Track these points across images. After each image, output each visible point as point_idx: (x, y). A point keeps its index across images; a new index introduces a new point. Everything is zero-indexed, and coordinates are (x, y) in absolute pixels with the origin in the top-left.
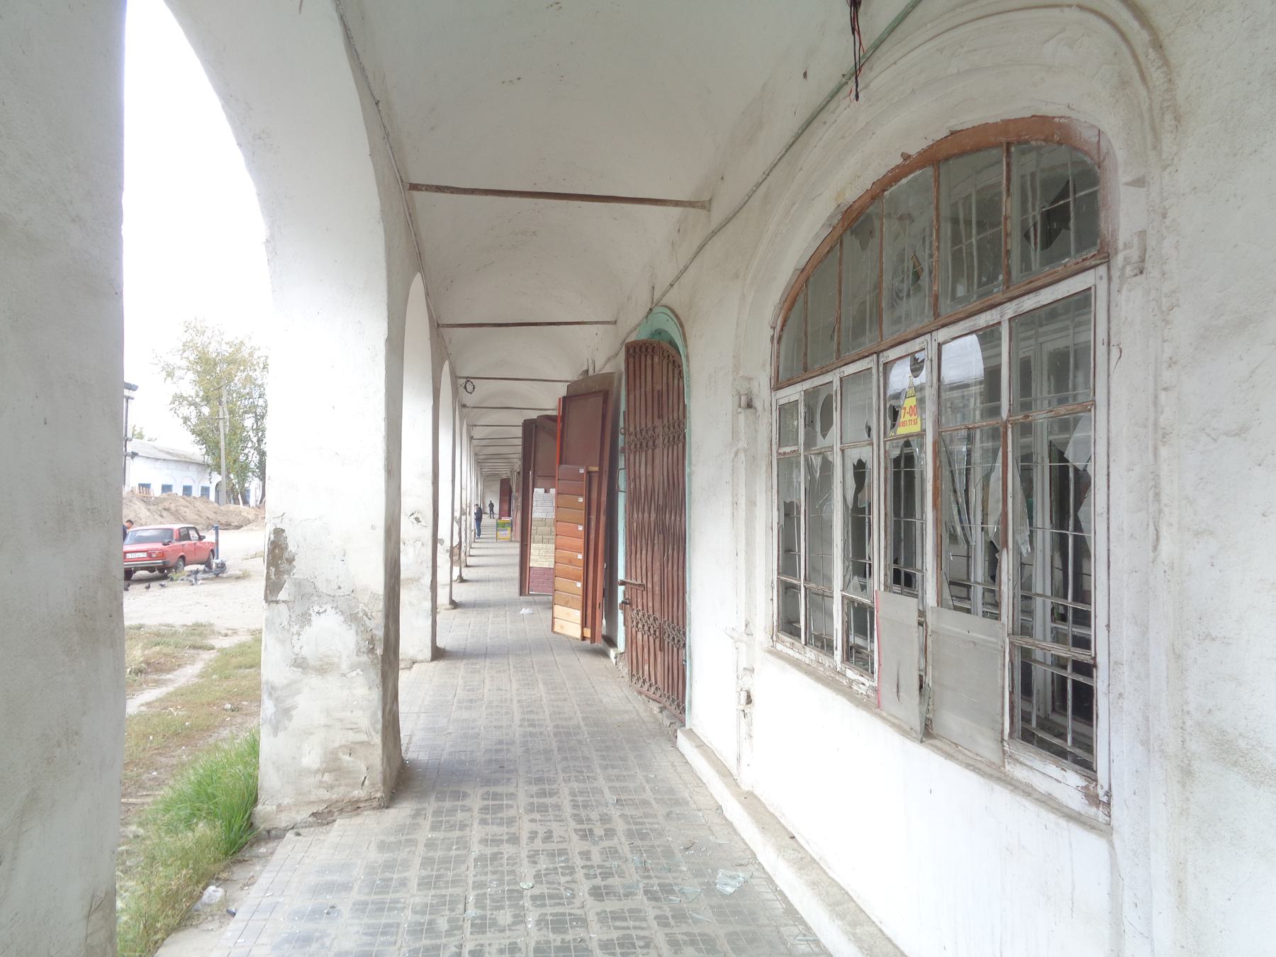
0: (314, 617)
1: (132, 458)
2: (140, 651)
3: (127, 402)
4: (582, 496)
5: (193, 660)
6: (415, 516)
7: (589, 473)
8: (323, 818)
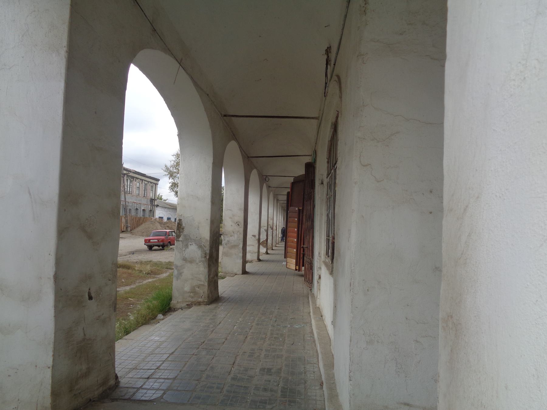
0: (189, 246)
1: (157, 207)
2: (149, 267)
3: (156, 185)
4: (296, 218)
5: (166, 272)
6: (238, 223)
7: (299, 210)
8: (189, 306)
